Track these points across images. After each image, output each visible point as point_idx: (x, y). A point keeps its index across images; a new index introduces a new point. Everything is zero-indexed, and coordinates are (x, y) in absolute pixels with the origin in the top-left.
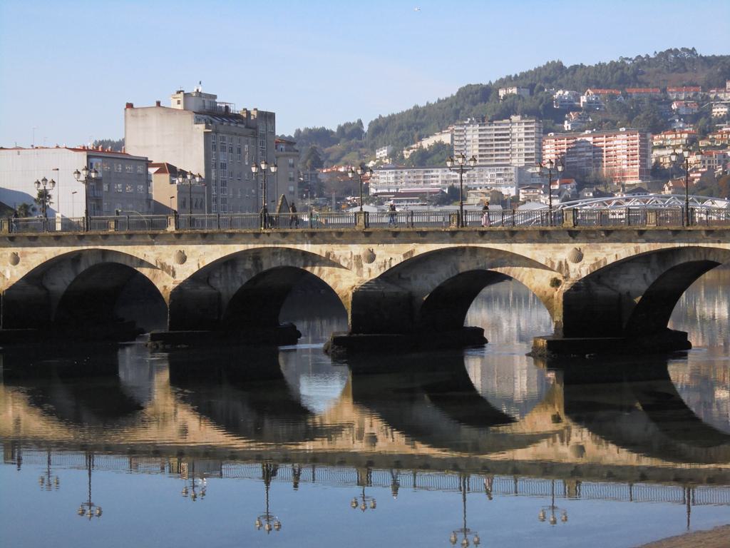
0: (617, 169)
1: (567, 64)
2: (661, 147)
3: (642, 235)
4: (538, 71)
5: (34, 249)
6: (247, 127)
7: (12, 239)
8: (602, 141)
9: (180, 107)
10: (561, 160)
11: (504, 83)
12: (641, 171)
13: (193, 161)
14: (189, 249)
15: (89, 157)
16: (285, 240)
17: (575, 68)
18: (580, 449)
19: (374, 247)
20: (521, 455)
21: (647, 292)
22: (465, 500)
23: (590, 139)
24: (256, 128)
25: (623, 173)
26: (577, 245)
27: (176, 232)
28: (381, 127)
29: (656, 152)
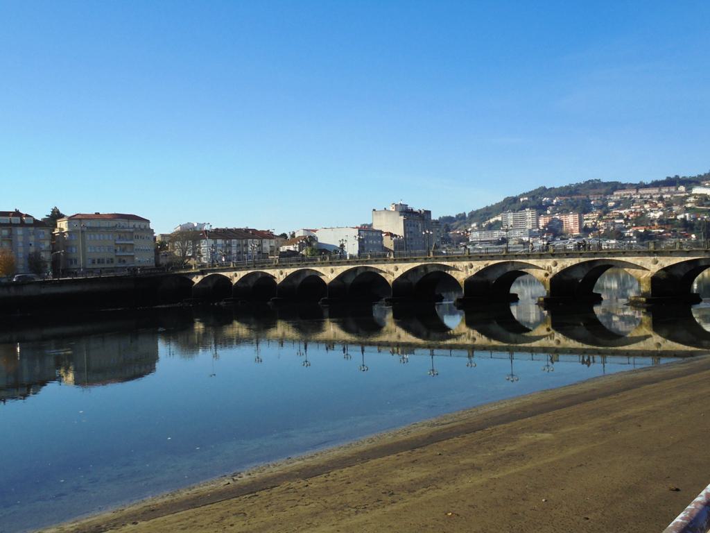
0: (569, 229)
2: (587, 219)
8: (563, 218)
9: (394, 210)
11: (522, 196)
13: (399, 231)
14: (399, 265)
17: (551, 189)
19: (472, 262)
23: (558, 217)
25: (572, 230)
26: (555, 259)
28: (474, 215)
29: (586, 222)
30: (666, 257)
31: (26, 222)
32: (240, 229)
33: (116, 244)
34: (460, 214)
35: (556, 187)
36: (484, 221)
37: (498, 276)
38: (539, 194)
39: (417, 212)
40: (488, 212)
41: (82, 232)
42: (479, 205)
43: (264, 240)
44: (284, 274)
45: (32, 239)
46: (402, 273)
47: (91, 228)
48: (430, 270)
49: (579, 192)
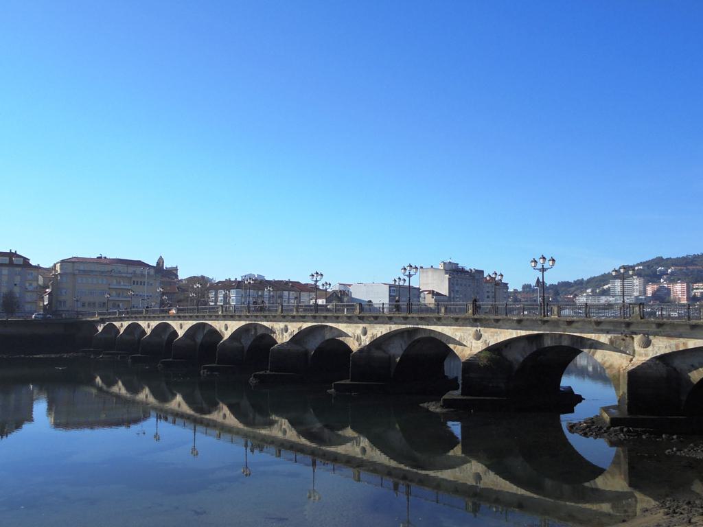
0: (677, 297)
1: (665, 258)
2: (697, 289)
3: (663, 328)
4: (653, 260)
5: (187, 322)
6: (471, 276)
7: (284, 317)
8: (671, 286)
9: (442, 268)
10: (654, 294)
11: (638, 265)
12: (687, 298)
13: (444, 290)
14: (229, 323)
15: (390, 287)
16: (423, 321)
17: (667, 259)
18: (364, 450)
19: (287, 323)
20: (341, 449)
21: (403, 355)
22: (314, 472)
23: (666, 285)
24: (474, 277)
25: (679, 298)
26: (365, 325)
27: (389, 315)
28: (590, 281)
29: (695, 291)
30: (493, 330)
31: (15, 262)
32: (282, 281)
33: (110, 288)
34: (578, 280)
35: (672, 257)
36: (599, 288)
37: (317, 346)
38: (656, 263)
39: (467, 272)
40: (605, 278)
41: (74, 275)
42: (598, 272)
43: (302, 293)
44: (369, 334)
45: (18, 279)
46: (663, 353)
47: (84, 271)
48: (548, 343)
49: (696, 262)
